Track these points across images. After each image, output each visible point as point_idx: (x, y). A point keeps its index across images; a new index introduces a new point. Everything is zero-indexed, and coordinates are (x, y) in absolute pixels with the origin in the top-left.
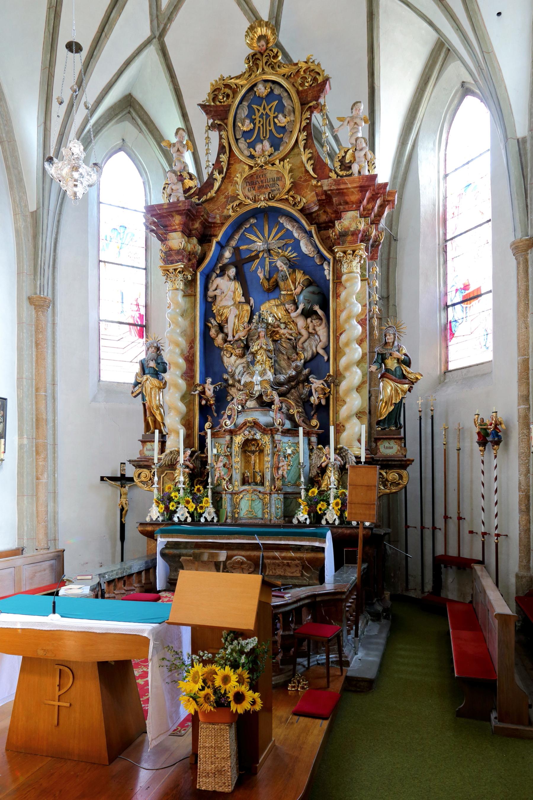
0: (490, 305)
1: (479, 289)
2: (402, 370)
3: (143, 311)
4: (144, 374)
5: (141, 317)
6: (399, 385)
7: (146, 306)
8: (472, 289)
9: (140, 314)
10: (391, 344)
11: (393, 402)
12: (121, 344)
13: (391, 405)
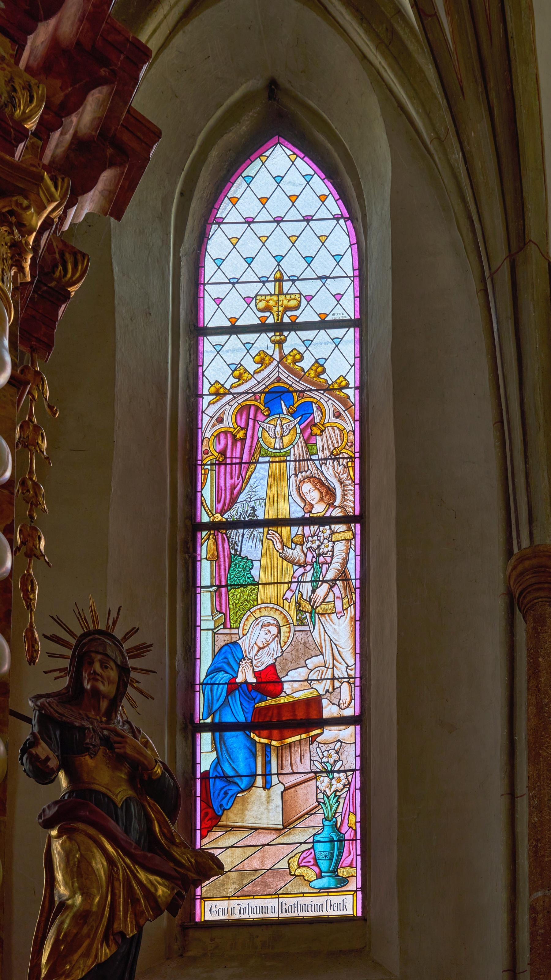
0: (350, 759)
1: (315, 702)
2: (149, 821)
6: (142, 875)
8: (293, 690)
10: (104, 705)
11: (118, 926)
13: (106, 938)
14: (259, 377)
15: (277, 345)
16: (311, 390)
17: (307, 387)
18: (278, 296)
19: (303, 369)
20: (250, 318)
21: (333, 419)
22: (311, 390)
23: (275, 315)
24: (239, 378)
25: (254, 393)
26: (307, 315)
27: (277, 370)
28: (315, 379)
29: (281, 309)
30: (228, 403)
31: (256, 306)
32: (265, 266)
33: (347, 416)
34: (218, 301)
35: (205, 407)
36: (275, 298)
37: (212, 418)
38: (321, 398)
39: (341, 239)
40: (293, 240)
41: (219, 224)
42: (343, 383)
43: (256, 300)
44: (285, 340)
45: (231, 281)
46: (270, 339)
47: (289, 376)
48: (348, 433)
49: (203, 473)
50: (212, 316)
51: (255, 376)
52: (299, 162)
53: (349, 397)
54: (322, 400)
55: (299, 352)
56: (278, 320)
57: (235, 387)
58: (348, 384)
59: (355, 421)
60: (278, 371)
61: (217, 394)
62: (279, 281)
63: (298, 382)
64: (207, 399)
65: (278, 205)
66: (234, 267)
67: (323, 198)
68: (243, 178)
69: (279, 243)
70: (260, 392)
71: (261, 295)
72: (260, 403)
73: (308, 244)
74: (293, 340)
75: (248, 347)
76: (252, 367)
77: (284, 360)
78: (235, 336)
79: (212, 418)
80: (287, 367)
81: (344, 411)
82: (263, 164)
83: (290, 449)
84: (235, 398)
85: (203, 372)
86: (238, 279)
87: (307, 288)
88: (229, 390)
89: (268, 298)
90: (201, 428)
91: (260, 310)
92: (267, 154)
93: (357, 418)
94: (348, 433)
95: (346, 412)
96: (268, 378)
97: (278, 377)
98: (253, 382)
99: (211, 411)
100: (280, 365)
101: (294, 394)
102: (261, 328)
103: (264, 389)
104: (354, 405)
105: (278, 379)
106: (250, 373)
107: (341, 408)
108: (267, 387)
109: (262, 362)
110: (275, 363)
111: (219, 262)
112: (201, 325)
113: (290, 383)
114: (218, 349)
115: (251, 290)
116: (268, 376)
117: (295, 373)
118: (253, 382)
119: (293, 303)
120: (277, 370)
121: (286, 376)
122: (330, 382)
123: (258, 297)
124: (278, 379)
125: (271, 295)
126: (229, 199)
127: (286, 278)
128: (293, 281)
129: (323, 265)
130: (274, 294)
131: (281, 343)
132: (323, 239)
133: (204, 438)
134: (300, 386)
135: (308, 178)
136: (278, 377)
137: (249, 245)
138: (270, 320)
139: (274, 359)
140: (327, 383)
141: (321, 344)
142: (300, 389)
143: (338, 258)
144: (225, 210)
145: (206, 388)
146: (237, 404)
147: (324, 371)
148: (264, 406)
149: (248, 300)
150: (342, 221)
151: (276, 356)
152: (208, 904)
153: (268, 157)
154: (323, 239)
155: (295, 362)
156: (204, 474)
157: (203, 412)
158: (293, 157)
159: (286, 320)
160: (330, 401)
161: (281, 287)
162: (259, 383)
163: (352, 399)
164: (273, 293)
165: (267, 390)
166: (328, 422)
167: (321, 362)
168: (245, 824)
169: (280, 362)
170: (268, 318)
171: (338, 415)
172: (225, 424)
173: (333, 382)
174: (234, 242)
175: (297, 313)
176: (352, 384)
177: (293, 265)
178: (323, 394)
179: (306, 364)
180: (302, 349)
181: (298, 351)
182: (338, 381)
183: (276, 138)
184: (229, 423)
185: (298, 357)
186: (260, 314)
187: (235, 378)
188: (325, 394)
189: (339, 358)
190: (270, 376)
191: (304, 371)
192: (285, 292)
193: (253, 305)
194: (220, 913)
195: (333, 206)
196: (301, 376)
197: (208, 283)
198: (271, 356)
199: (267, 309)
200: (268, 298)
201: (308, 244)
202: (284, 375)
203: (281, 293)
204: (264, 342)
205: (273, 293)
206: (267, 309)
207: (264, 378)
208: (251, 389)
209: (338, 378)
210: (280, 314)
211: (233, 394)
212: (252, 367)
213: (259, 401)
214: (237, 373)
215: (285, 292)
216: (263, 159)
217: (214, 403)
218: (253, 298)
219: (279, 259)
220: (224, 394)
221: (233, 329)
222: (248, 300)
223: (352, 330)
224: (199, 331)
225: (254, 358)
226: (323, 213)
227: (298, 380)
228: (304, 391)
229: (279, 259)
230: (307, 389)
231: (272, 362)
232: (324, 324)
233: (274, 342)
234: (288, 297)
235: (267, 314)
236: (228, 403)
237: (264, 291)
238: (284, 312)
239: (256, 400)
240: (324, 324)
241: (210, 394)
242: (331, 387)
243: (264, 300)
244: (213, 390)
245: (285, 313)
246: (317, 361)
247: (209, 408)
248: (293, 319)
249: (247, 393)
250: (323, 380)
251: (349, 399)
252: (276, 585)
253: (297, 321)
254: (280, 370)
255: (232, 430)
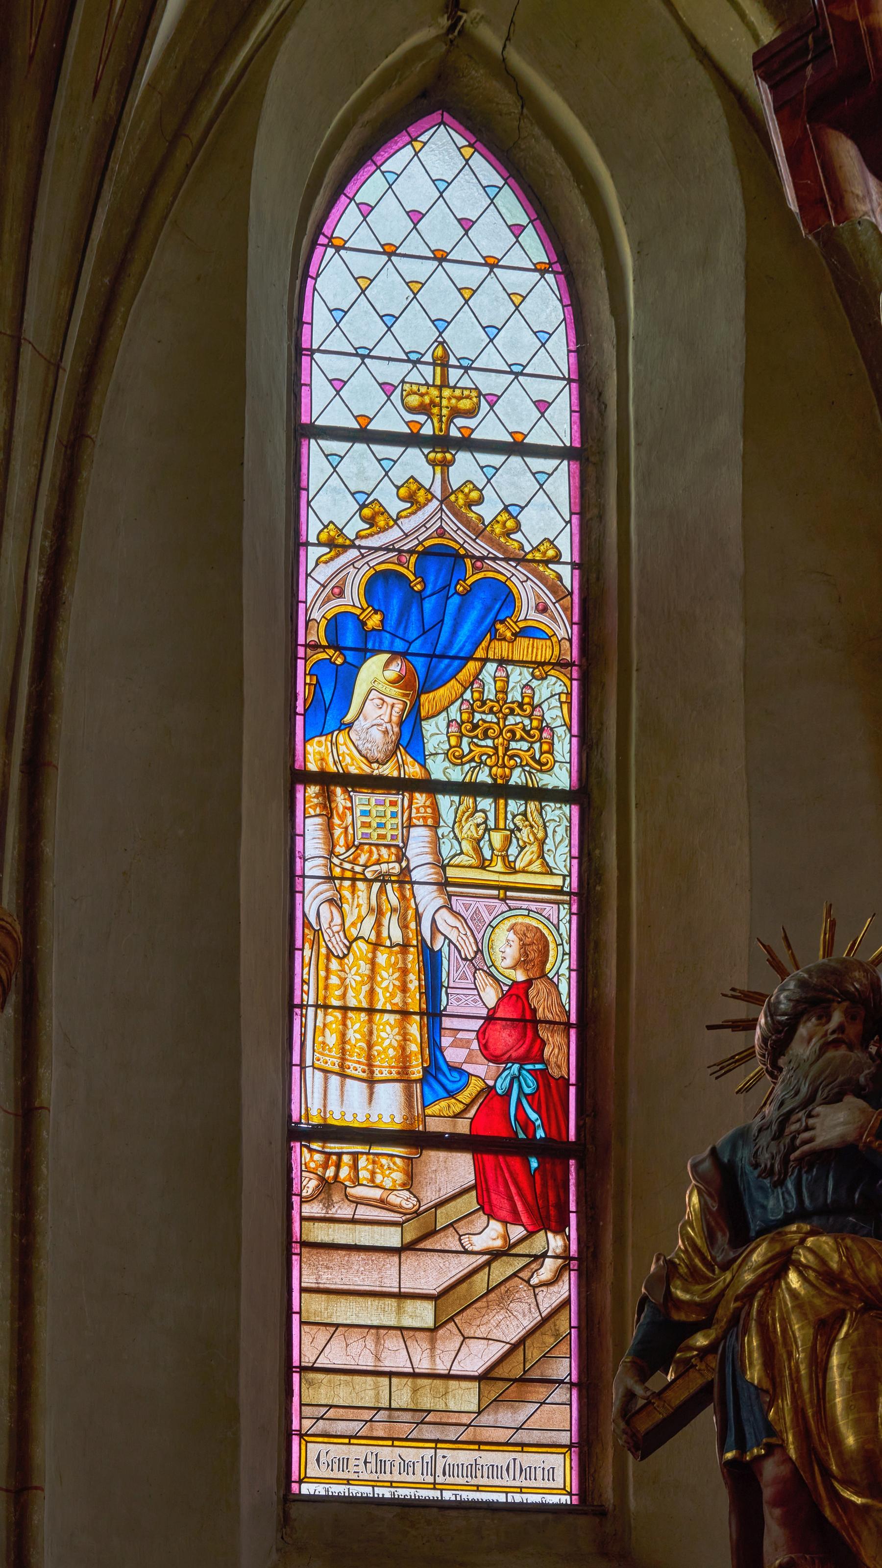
3: (561, 1053)
4: (742, 1238)
5: (549, 1092)
7: (589, 1022)
9: (543, 1077)
12: (430, 1273)
14: (408, 525)
15: (438, 469)
16: (495, 559)
17: (490, 552)
18: (440, 388)
19: (481, 519)
20: (392, 420)
21: (533, 615)
22: (495, 559)
23: (436, 420)
24: (371, 521)
25: (400, 551)
26: (488, 429)
27: (439, 515)
28: (502, 540)
29: (445, 412)
30: (353, 564)
31: (402, 400)
32: (417, 334)
33: (557, 609)
34: (338, 385)
35: (311, 566)
36: (434, 392)
37: (324, 586)
38: (513, 574)
39: (547, 305)
40: (467, 294)
41: (338, 249)
42: (551, 553)
43: (402, 390)
44: (453, 462)
45: (360, 351)
46: (426, 456)
47: (459, 528)
48: (559, 641)
49: (308, 681)
50: (323, 406)
51: (399, 522)
52: (479, 162)
53: (560, 578)
54: (513, 579)
55: (476, 488)
56: (441, 430)
57: (366, 537)
58: (559, 554)
59: (572, 624)
60: (441, 518)
61: (331, 544)
62: (442, 363)
63: (474, 540)
64: (314, 553)
65: (440, 231)
66: (363, 328)
67: (517, 230)
68: (383, 173)
69: (441, 297)
70: (411, 552)
71: (411, 383)
72: (408, 568)
73: (491, 304)
74: (465, 467)
75: (386, 467)
76: (394, 506)
77: (453, 498)
78: (365, 446)
79: (324, 586)
80: (457, 514)
81: (554, 604)
82: (416, 154)
83: (473, 574)
84: (363, 556)
85: (308, 504)
86: (371, 350)
87: (488, 384)
88: (353, 541)
89: (423, 390)
90: (305, 602)
91: (411, 410)
92: (424, 138)
93: (576, 619)
94: (559, 641)
95: (557, 605)
96: (424, 529)
97: (441, 527)
98: (394, 534)
99: (323, 573)
100: (444, 507)
101: (468, 562)
102: (411, 440)
103: (417, 546)
104: (571, 594)
105: (441, 533)
106: (391, 517)
107: (548, 598)
108: (421, 543)
109: (411, 499)
110: (435, 504)
111: (339, 314)
112: (305, 419)
113: (461, 542)
114: (334, 461)
115: (394, 373)
116: (424, 525)
117: (467, 523)
118: (394, 534)
119: (465, 404)
120: (439, 515)
121: (455, 528)
122: (528, 548)
123: (407, 387)
124: (441, 533)
125: (427, 384)
126: (358, 205)
127: (453, 361)
128: (466, 369)
129: (517, 344)
130: (434, 385)
131: (446, 465)
132: (517, 300)
133: (309, 620)
134: (480, 548)
135: (492, 192)
136: (441, 527)
137: (389, 292)
138: (427, 430)
139: (434, 496)
140: (523, 550)
141: (514, 478)
142: (477, 554)
143: (543, 338)
144: (346, 223)
145: (313, 530)
146: (366, 567)
147: (518, 527)
148: (415, 574)
149: (387, 388)
150: (550, 277)
151: (437, 490)
152: (314, 1449)
153: (425, 144)
154: (517, 300)
155: (469, 505)
156: (310, 684)
157: (308, 575)
158: (468, 151)
159: (454, 432)
160: (529, 582)
161: (445, 377)
162: (407, 535)
163: (567, 582)
164: (431, 383)
165: (420, 548)
166: (525, 619)
167: (514, 510)
168: (384, 1289)
169: (444, 500)
170: (422, 425)
171: (543, 609)
172: (347, 600)
173: (534, 549)
174: (364, 283)
175: (471, 423)
176: (566, 557)
177: (464, 340)
178: (515, 567)
179: (488, 511)
180: (480, 482)
181: (474, 486)
182: (542, 548)
183: (436, 116)
184: (353, 599)
185: (474, 495)
186: (409, 417)
187: (364, 519)
188: (518, 567)
189: (542, 509)
190: (428, 526)
191: (483, 523)
192: (452, 384)
193: (396, 396)
194: (336, 1466)
195: (534, 247)
196: (479, 531)
197: (319, 350)
198: (428, 491)
199: (422, 409)
200: (423, 390)
201: (491, 304)
202: (451, 524)
203: (445, 384)
204: (415, 463)
205: (431, 383)
206: (422, 409)
207: (415, 527)
208: (393, 545)
209: (542, 543)
210: (444, 419)
211: (359, 547)
212: (394, 506)
213: (406, 565)
214: (367, 512)
215: (452, 384)
216: (418, 145)
217: (326, 562)
218: (396, 387)
219: (440, 324)
220: (345, 548)
221: (363, 435)
222: (387, 388)
223: (565, 462)
224: (303, 432)
225: (398, 488)
226: (516, 258)
227: (474, 537)
228: (482, 559)
229: (440, 324)
230: (490, 555)
231: (430, 501)
232: (518, 447)
233: (433, 463)
234: (458, 392)
235: (422, 418)
236: (353, 564)
237: (414, 377)
238: (450, 420)
239: (400, 564)
240: (518, 447)
241: (320, 544)
242: (529, 557)
243: (415, 393)
244: (324, 537)
245: (452, 421)
246: (506, 509)
247: (318, 570)
248: (466, 433)
249: (387, 549)
250: (516, 544)
251: (561, 581)
252: (369, 1379)
253: (472, 436)
254: (444, 517)
255: (358, 612)
